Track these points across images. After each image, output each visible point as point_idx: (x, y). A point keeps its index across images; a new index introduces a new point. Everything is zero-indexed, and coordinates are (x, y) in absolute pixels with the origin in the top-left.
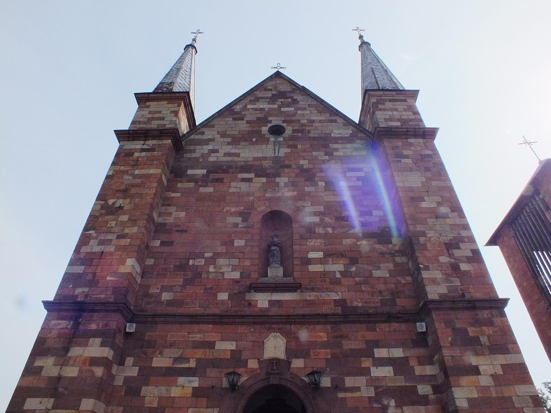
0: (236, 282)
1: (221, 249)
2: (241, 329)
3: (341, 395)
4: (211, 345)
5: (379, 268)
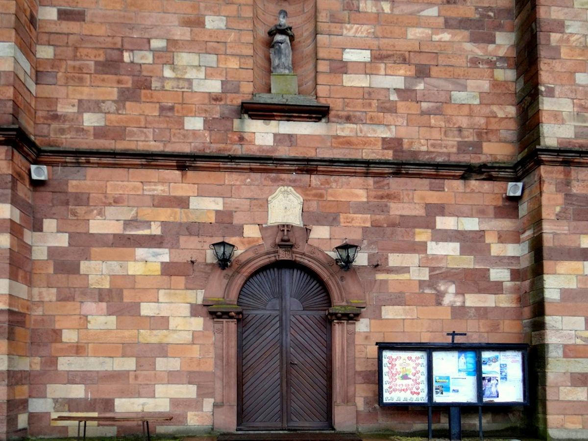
0: (216, 98)
1: (182, 33)
2: (231, 179)
3: (380, 277)
4: (183, 203)
5: (464, 88)
